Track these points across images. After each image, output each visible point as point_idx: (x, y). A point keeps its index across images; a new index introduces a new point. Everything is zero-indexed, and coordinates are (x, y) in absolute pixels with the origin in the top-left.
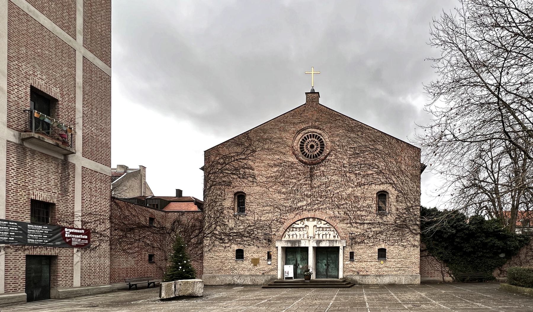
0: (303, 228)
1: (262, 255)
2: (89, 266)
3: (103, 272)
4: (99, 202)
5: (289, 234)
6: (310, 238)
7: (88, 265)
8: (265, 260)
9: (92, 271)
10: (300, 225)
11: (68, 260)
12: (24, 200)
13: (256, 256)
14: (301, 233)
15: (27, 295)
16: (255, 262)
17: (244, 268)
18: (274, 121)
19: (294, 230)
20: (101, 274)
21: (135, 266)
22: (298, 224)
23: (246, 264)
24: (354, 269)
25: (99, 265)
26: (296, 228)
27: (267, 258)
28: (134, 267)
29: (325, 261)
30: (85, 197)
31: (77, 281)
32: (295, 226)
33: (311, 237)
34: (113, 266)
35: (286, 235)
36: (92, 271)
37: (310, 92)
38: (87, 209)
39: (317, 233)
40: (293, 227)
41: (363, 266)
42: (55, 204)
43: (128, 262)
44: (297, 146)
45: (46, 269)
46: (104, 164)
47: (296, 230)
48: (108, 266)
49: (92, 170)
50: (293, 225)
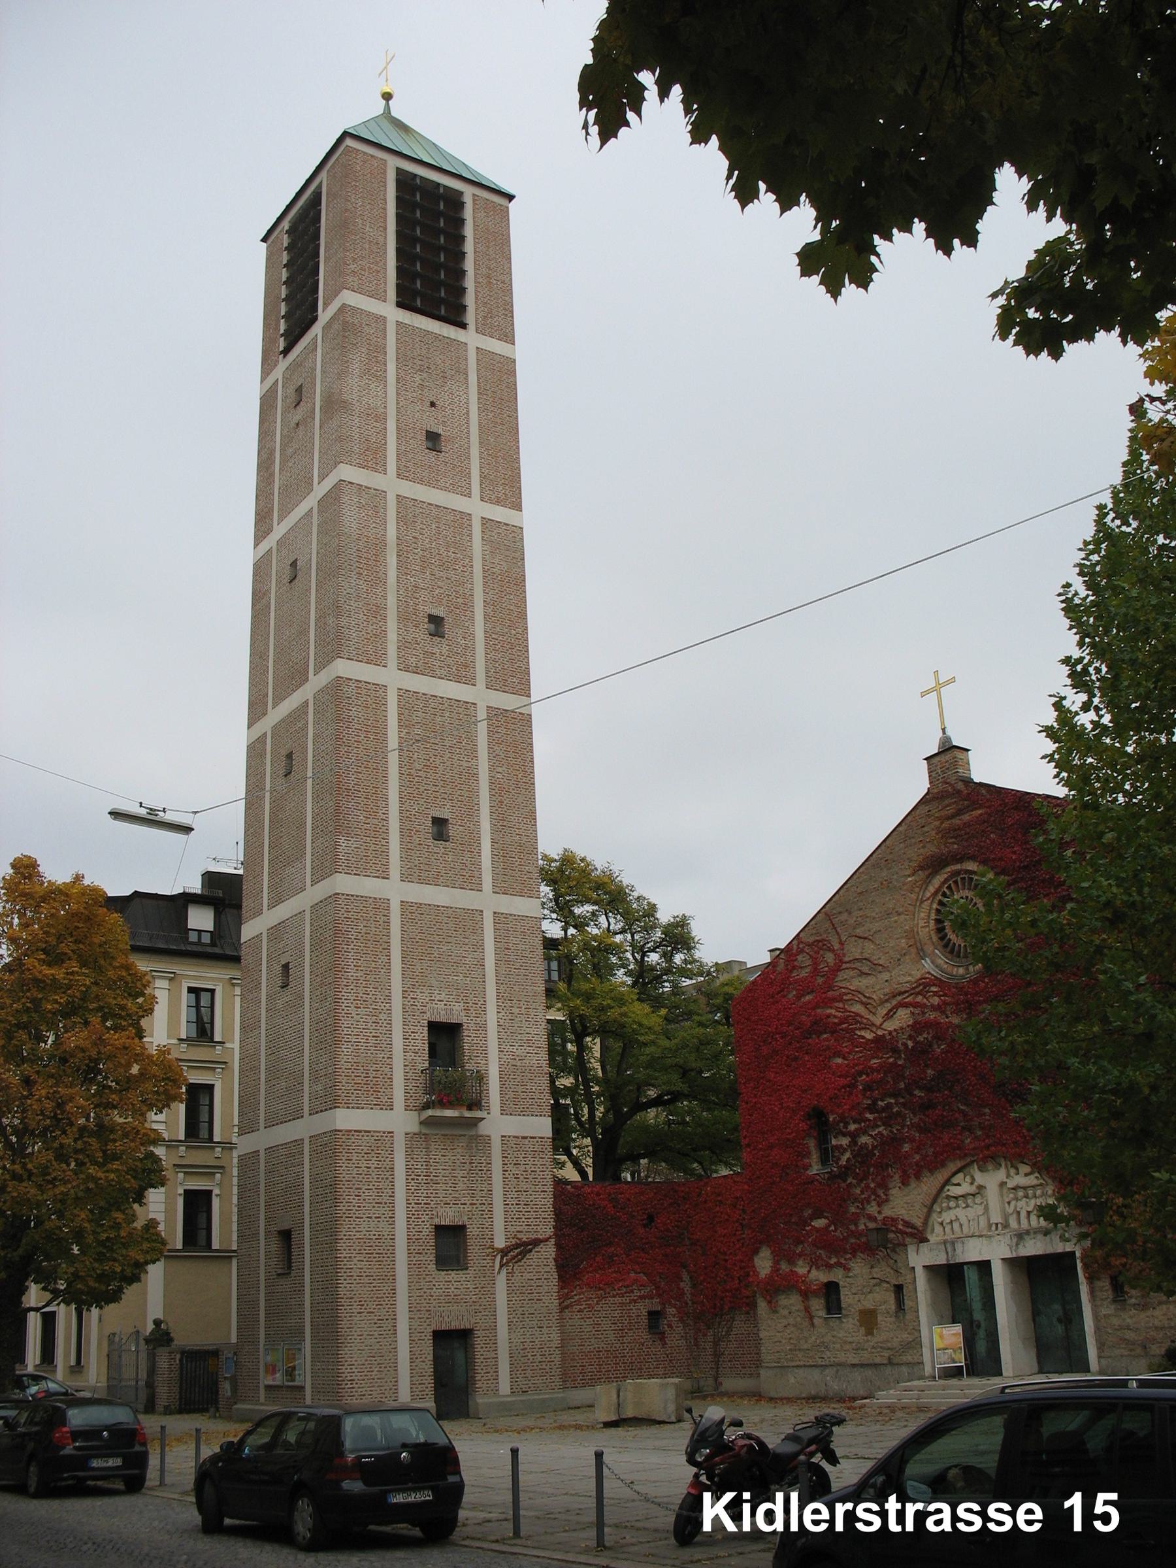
0: (973, 1195)
1: (883, 1299)
2: (523, 1350)
3: (549, 1362)
4: (534, 1203)
5: (940, 1220)
6: (994, 1228)
7: (522, 1347)
8: (891, 1313)
9: (529, 1359)
10: (965, 1188)
11: (488, 1337)
12: (427, 1231)
13: (868, 1304)
14: (970, 1212)
15: (437, 1406)
16: (868, 1319)
17: (845, 1342)
18: (866, 869)
19: (952, 1204)
20: (544, 1367)
21: (617, 1345)
22: (959, 1185)
23: (849, 1328)
24: (1129, 1335)
25: (541, 1345)
26: (956, 1198)
27: (893, 1307)
28: (615, 1347)
29: (1057, 1307)
30: (510, 1199)
31: (505, 1387)
32: (954, 1191)
33: (997, 1224)
34: (569, 1348)
35: (935, 1223)
36: (529, 1359)
37: (937, 751)
38: (513, 1223)
39: (1010, 1210)
40: (948, 1197)
41: (1157, 1323)
42: (465, 1226)
43: (600, 1336)
44: (928, 926)
45: (460, 1356)
46: (537, 1116)
47: (957, 1206)
48: (556, 1348)
49: (518, 1137)
50: (947, 1187)
